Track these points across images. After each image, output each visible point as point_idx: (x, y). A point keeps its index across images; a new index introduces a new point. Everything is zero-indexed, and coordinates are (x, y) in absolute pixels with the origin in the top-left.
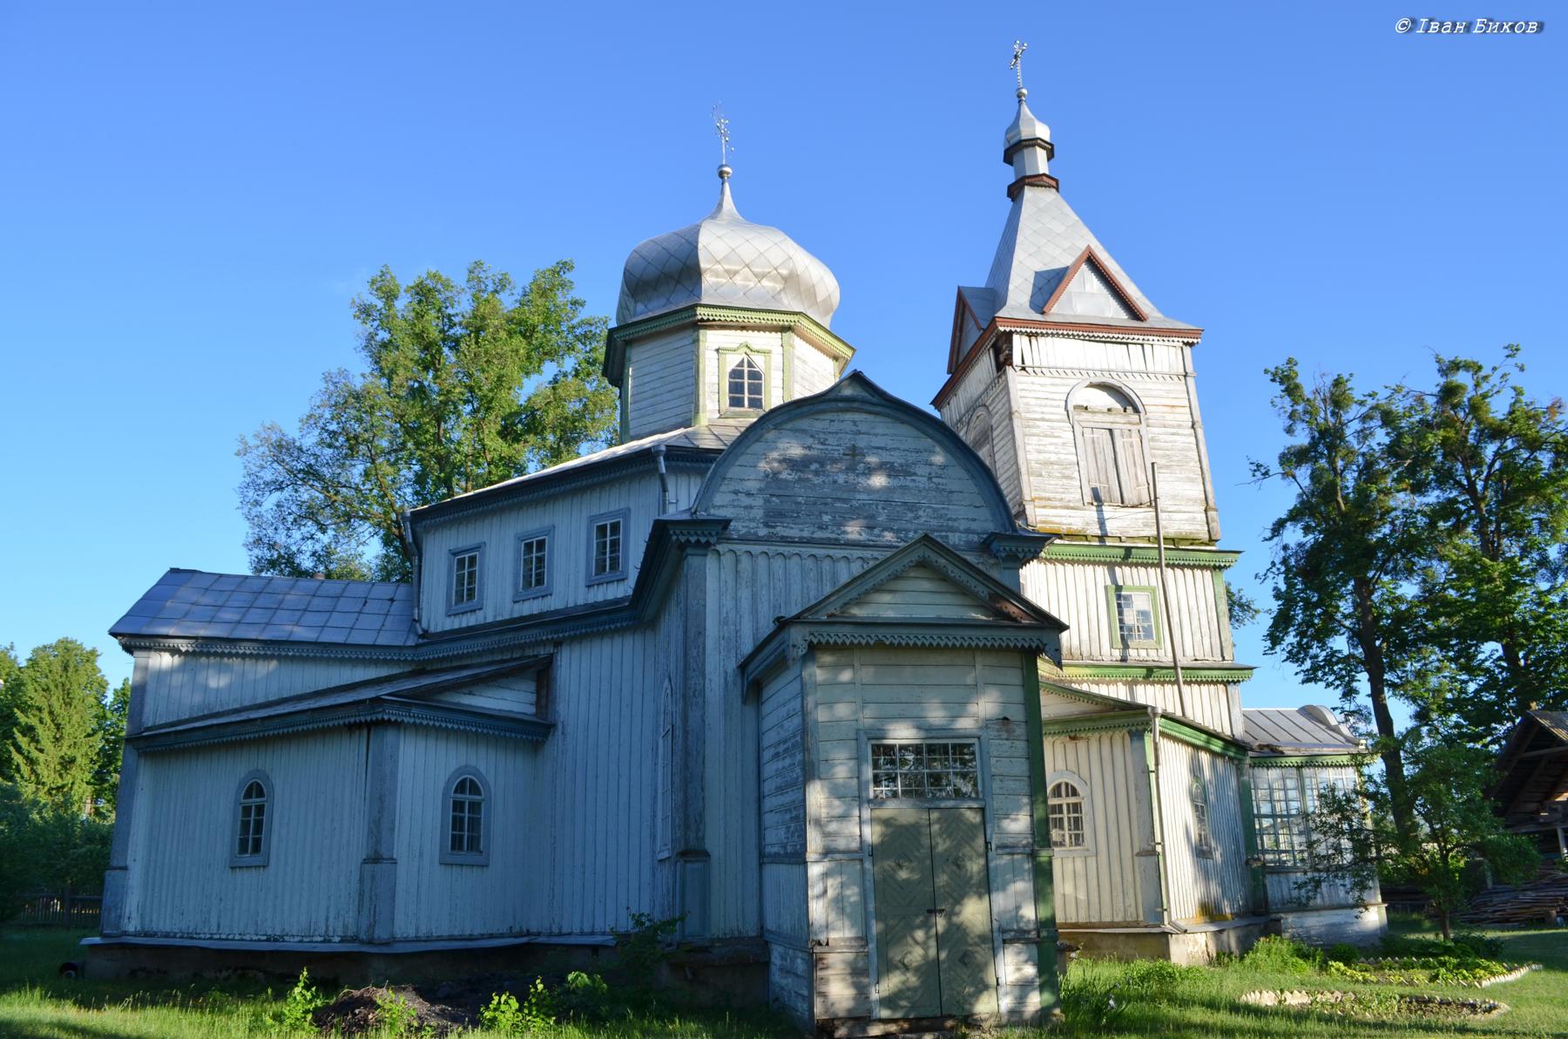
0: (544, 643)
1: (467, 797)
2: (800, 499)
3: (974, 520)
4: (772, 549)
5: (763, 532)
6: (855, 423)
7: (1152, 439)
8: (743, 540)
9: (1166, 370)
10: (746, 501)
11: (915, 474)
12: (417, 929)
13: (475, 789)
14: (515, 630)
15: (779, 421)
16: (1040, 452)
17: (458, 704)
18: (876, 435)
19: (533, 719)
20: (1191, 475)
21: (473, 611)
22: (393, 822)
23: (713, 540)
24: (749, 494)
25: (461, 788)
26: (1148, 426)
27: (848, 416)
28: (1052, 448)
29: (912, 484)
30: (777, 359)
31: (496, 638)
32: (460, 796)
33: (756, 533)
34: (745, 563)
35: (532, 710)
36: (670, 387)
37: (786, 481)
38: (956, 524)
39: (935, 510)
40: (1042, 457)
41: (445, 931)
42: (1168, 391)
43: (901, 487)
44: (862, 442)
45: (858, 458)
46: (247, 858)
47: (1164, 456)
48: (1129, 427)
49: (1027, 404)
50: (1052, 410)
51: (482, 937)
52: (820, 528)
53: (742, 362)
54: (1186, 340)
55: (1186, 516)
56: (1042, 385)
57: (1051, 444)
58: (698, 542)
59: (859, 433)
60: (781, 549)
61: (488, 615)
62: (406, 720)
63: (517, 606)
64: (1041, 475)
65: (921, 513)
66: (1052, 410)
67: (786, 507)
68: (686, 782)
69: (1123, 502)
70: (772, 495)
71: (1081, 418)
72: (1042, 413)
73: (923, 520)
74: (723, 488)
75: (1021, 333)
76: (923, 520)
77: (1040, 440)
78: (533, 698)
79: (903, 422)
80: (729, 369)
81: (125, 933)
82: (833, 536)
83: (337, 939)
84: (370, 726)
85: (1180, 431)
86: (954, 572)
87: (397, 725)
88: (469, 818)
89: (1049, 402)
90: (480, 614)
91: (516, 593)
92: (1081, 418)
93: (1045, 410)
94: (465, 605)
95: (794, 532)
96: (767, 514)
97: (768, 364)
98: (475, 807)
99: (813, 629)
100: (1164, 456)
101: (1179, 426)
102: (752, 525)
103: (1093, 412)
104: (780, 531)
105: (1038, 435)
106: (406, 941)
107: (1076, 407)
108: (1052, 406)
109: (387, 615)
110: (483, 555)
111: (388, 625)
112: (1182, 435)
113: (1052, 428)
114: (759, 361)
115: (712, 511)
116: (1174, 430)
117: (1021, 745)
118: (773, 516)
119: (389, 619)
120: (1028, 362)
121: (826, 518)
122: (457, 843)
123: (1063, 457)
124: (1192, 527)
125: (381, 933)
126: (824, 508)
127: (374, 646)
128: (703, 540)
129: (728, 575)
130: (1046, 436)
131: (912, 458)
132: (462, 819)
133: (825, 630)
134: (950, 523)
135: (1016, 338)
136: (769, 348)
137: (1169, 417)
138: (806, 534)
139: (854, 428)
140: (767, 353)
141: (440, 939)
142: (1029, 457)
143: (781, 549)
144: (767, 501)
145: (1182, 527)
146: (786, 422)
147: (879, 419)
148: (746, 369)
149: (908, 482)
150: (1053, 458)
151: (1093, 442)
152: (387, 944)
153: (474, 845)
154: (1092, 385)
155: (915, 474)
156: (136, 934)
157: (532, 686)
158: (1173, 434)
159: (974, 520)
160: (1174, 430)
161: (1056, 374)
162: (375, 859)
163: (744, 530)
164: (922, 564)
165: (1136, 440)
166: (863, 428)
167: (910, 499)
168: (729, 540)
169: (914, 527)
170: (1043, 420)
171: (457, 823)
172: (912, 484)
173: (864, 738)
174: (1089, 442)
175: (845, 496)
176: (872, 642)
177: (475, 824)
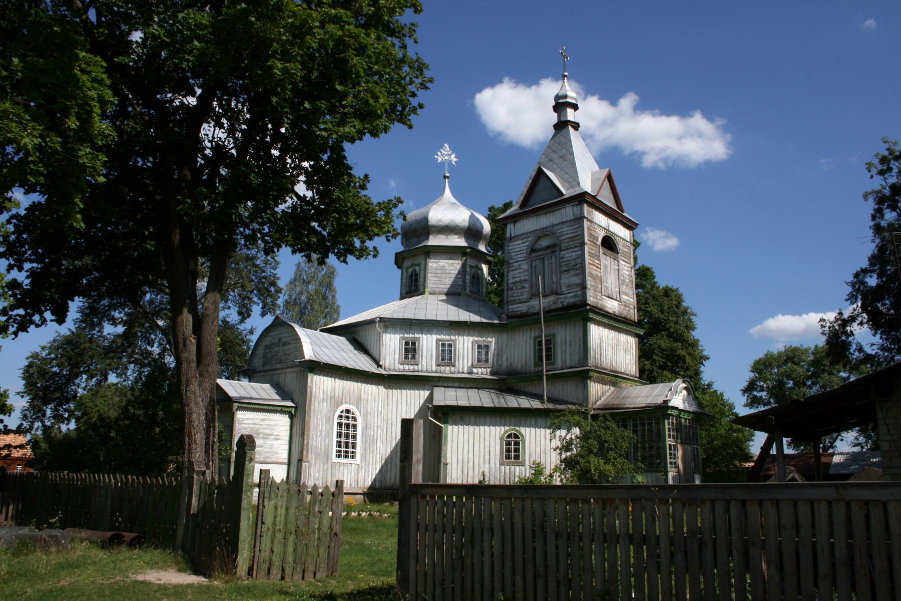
9: (572, 217)
13: (516, 436)
16: (513, 278)
20: (578, 272)
40: (514, 280)
42: (574, 229)
93: (518, 256)
97: (420, 269)
98: (517, 444)
101: (576, 247)
114: (417, 268)
118: (265, 364)
150: (518, 279)
153: (517, 457)
170: (517, 262)
174: (534, 268)
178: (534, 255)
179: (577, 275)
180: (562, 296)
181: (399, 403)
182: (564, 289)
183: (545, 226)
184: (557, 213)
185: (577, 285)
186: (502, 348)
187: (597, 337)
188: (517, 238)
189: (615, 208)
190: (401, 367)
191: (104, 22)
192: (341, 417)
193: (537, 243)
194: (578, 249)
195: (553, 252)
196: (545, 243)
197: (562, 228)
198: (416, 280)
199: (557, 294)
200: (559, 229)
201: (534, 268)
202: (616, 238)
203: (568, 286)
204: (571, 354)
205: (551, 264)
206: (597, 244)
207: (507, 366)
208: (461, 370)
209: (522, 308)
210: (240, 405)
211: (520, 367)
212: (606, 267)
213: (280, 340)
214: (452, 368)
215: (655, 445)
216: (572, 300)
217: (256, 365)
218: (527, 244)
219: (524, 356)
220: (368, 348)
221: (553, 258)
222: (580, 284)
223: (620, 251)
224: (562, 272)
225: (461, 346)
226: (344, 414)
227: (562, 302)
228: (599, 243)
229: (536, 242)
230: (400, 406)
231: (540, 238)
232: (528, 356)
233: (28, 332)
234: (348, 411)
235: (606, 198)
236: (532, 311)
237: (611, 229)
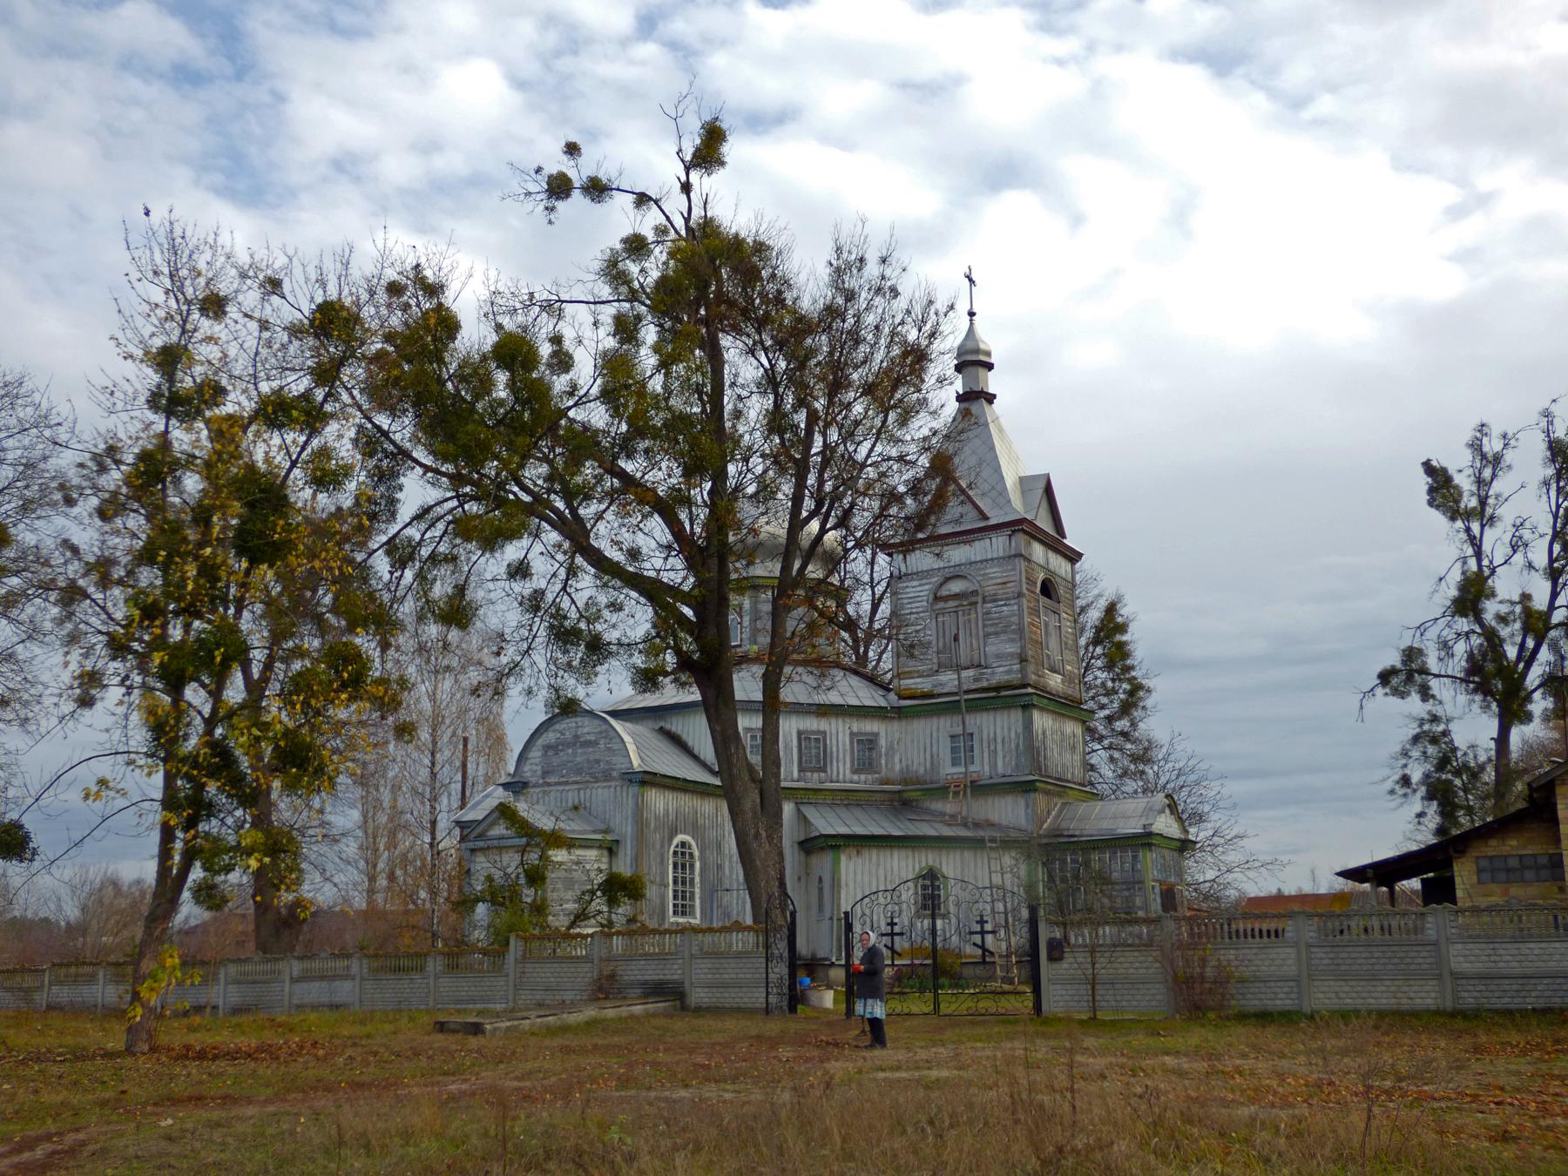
7: (987, 613)
9: (1001, 555)
101: (1008, 599)
118: (545, 773)
170: (911, 613)
174: (940, 625)
178: (941, 605)
179: (1012, 640)
180: (989, 671)
182: (990, 660)
184: (977, 544)
185: (1012, 655)
186: (892, 742)
187: (1040, 732)
189: (1052, 532)
190: (856, 777)
191: (532, 411)
192: (675, 853)
193: (944, 588)
195: (971, 604)
196: (956, 587)
197: (986, 568)
199: (979, 666)
200: (979, 569)
201: (940, 625)
202: (1058, 579)
203: (999, 656)
204: (1004, 757)
205: (969, 621)
206: (1034, 593)
207: (901, 771)
211: (922, 770)
212: (1047, 625)
213: (576, 737)
214: (823, 775)
215: (1061, 886)
217: (528, 774)
218: (927, 587)
219: (928, 757)
220: (690, 744)
221: (973, 612)
223: (1062, 599)
224: (986, 635)
225: (834, 742)
226: (679, 849)
228: (1038, 590)
229: (941, 585)
231: (947, 580)
233: (1279, 890)
234: (683, 844)
235: (1045, 523)
237: (1051, 567)
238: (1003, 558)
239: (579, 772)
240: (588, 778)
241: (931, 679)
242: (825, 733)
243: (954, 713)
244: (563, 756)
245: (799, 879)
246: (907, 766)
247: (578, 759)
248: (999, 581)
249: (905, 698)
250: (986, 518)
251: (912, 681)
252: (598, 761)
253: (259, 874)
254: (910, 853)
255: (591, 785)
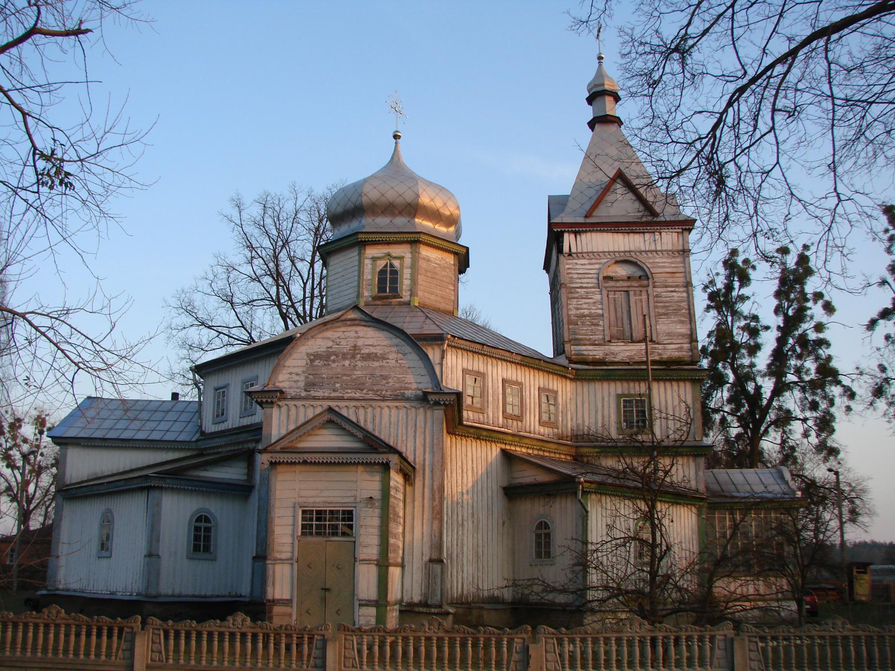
0: (251, 441)
1: (203, 525)
2: (324, 376)
3: (420, 383)
4: (307, 403)
5: (303, 394)
6: (356, 332)
7: (657, 296)
8: (293, 399)
9: (670, 248)
10: (296, 378)
11: (389, 359)
12: (173, 591)
13: (207, 520)
14: (237, 434)
15: (314, 334)
16: (577, 309)
17: (198, 476)
18: (368, 338)
19: (245, 483)
20: (682, 319)
21: (223, 422)
22: (159, 536)
23: (275, 400)
24: (297, 374)
25: (199, 519)
26: (654, 287)
27: (354, 328)
28: (585, 306)
29: (386, 365)
30: (408, 261)
31: (229, 438)
32: (198, 524)
33: (300, 395)
34: (293, 411)
35: (245, 477)
36: (346, 282)
37: (317, 366)
38: (410, 386)
39: (399, 378)
40: (578, 312)
41: (190, 592)
42: (672, 263)
43: (380, 366)
44: (360, 343)
45: (357, 352)
46: (104, 553)
47: (663, 307)
48: (640, 289)
49: (572, 278)
50: (587, 280)
51: (212, 596)
52: (334, 391)
53: (386, 266)
54: (684, 227)
55: (677, 346)
56: (582, 265)
57: (586, 303)
58: (267, 401)
59: (359, 337)
60: (312, 403)
61: (229, 425)
62: (164, 486)
63: (241, 420)
64: (577, 324)
65: (390, 380)
66: (587, 280)
67: (317, 380)
68: (152, 531)
69: (632, 340)
70: (309, 374)
71: (607, 285)
72: (581, 283)
73: (391, 384)
74: (284, 372)
75: (568, 232)
76: (391, 384)
77: (578, 301)
78: (246, 471)
79: (383, 330)
80: (378, 270)
81: (58, 589)
82: (340, 395)
83: (135, 594)
84: (149, 489)
85: (677, 289)
86: (347, 427)
87: (161, 488)
88: (204, 536)
89: (587, 276)
90: (226, 423)
91: (241, 414)
92: (607, 285)
93: (583, 281)
94: (219, 419)
95: (320, 394)
96: (306, 385)
97: (402, 265)
98: (207, 530)
99: (272, 455)
100: (663, 307)
101: (677, 286)
102: (298, 390)
103: (617, 281)
104: (313, 393)
105: (577, 298)
106: (167, 596)
107: (605, 278)
108: (588, 278)
109: (190, 422)
110: (228, 390)
111: (187, 429)
112: (678, 292)
113: (587, 293)
114: (396, 263)
115: (278, 384)
116: (673, 289)
117: (377, 512)
118: (309, 385)
119: (190, 424)
120: (574, 250)
121: (338, 385)
122: (196, 548)
123: (593, 311)
124: (680, 353)
125: (153, 592)
126: (337, 380)
127: (175, 441)
128: (269, 400)
129: (284, 417)
130: (582, 298)
131: (387, 350)
132: (200, 536)
133: (278, 455)
134: (407, 385)
135: (566, 236)
136: (403, 255)
137: (670, 280)
138: (326, 394)
139: (356, 335)
140: (401, 258)
141: (187, 596)
142: (570, 313)
143: (312, 403)
144: (307, 378)
145: (673, 353)
146: (318, 333)
147: (369, 329)
148: (389, 269)
149: (384, 363)
150: (586, 312)
151: (615, 301)
152: (155, 597)
153: (207, 549)
154: (617, 262)
155: (389, 359)
156: (63, 590)
157: (245, 465)
158: (672, 291)
159: (420, 383)
160: (673, 289)
161: (593, 257)
162: (150, 555)
163: (294, 394)
164: (330, 422)
165: (644, 297)
166: (361, 334)
167: (384, 373)
168: (285, 399)
169: (385, 388)
170: (581, 287)
171: (197, 538)
172: (386, 365)
173: (297, 507)
174: (611, 301)
175: (348, 373)
176: (301, 461)
177: (207, 539)
179: (682, 322)
180: (660, 346)
181: (465, 470)
183: (627, 249)
185: (683, 335)
188: (580, 255)
190: (542, 430)
194: (681, 289)
197: (655, 258)
198: (394, 281)
203: (669, 334)
205: (641, 301)
208: (528, 429)
209: (597, 352)
210: (335, 418)
216: (676, 354)
222: (687, 334)
227: (660, 354)
230: (465, 475)
232: (606, 419)
236: (610, 358)
238: (672, 251)
239: (360, 387)
240: (371, 395)
241: (602, 348)
242: (556, 392)
243: (639, 381)
244: (336, 367)
245: (504, 523)
246: (578, 426)
247: (358, 373)
248: (668, 270)
249: (575, 363)
250: (654, 214)
251: (584, 348)
252: (385, 377)
253: (55, 477)
254: (140, 495)
255: (374, 404)
